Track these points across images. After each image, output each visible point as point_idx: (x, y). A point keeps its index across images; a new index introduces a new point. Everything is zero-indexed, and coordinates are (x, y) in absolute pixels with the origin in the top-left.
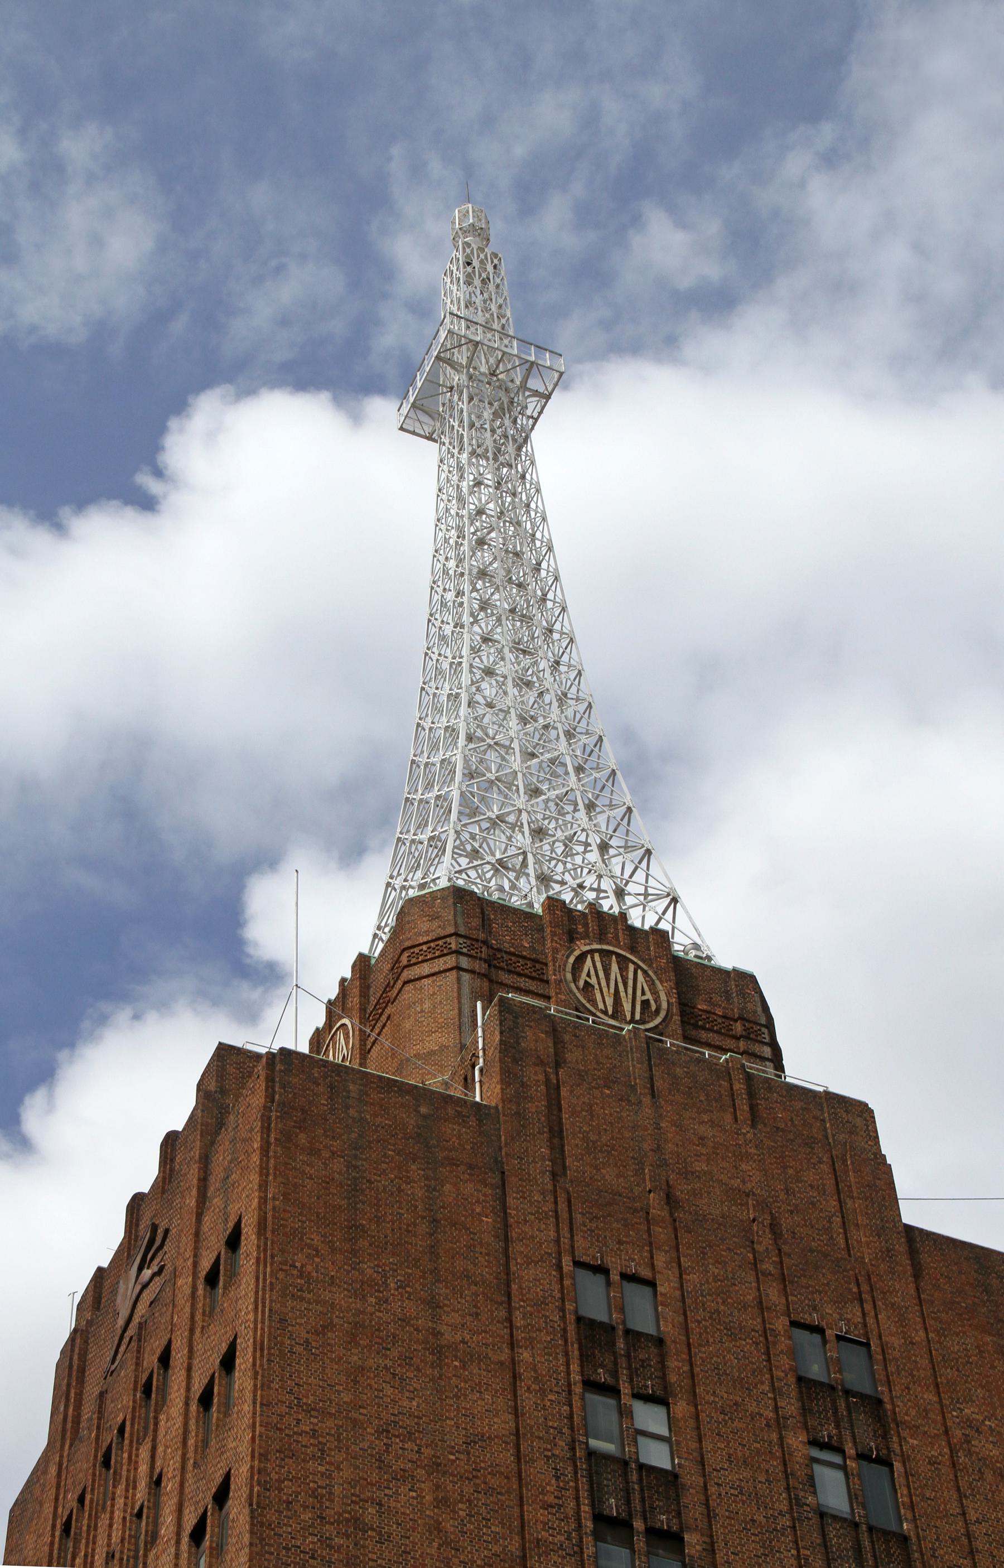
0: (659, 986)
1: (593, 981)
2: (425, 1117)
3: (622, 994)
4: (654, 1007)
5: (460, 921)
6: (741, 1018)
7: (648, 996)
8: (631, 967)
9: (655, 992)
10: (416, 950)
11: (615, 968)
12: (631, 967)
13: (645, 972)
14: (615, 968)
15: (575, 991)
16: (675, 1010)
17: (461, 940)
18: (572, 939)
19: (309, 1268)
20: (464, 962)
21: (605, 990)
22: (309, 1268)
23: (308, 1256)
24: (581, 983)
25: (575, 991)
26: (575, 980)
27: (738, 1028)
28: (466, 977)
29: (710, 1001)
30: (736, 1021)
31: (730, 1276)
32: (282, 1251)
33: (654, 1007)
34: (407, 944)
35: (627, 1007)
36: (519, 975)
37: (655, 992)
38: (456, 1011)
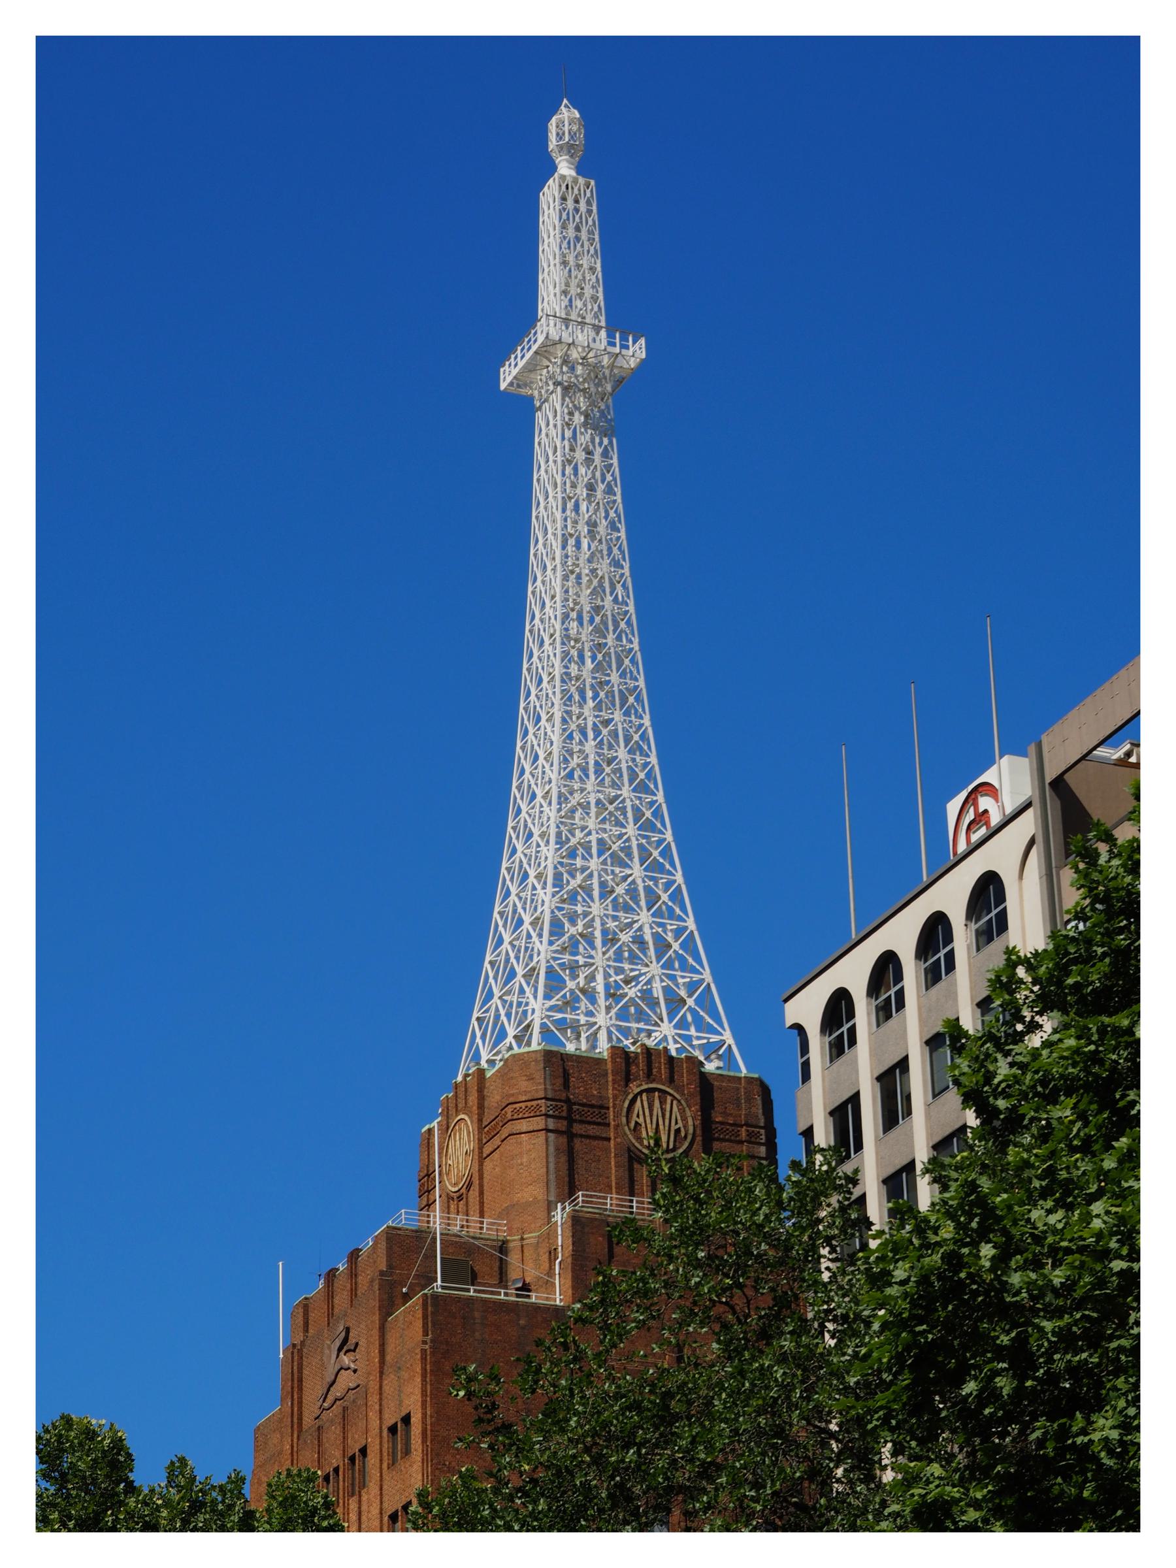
0: (688, 1113)
1: (641, 1120)
2: (523, 1328)
3: (661, 1127)
4: (683, 1134)
5: (548, 1082)
6: (747, 1125)
7: (680, 1124)
8: (669, 1098)
9: (684, 1119)
10: (517, 1106)
11: (657, 1103)
12: (669, 1098)
13: (679, 1101)
14: (657, 1103)
15: (628, 1132)
16: (699, 1132)
17: (549, 1103)
18: (628, 1080)
19: (453, 1464)
20: (551, 1124)
21: (649, 1126)
22: (453, 1464)
23: (454, 1456)
24: (632, 1125)
25: (628, 1132)
26: (628, 1122)
27: (743, 1132)
28: (552, 1136)
29: (724, 1114)
30: (742, 1126)
31: (514, 1448)
32: (438, 1455)
33: (683, 1134)
34: (512, 1100)
35: (664, 1138)
36: (589, 1123)
37: (684, 1119)
38: (545, 1170)
